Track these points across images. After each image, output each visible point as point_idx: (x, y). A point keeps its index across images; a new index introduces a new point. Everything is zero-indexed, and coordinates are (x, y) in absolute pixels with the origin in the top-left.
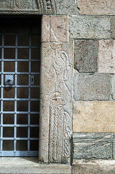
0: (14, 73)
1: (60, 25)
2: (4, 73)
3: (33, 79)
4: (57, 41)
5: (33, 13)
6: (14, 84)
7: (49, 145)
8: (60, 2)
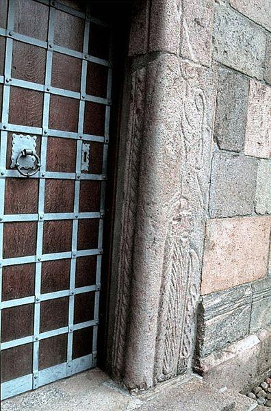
0: (38, 131)
1: (200, 16)
2: (11, 127)
3: (87, 156)
4: (193, 57)
7: (158, 339)
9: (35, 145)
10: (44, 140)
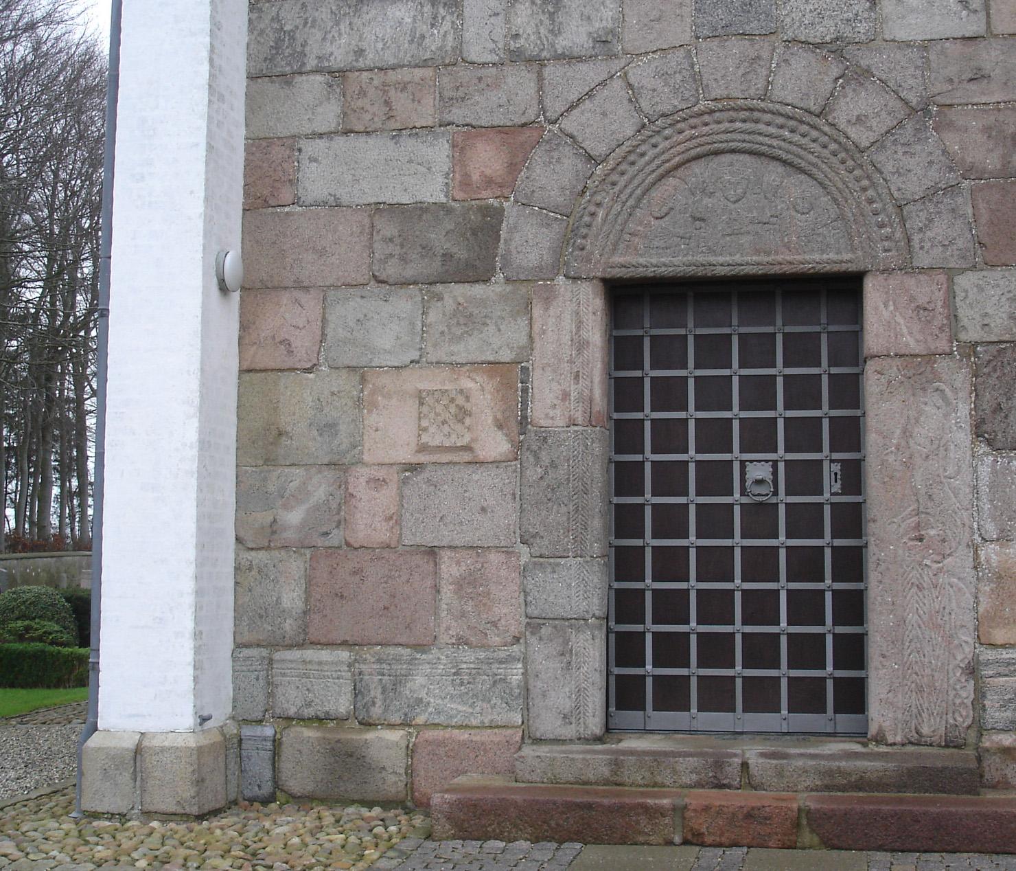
3: (839, 477)
5: (836, 268)
6: (776, 493)
8: (920, 230)
9: (771, 470)
10: (781, 466)
